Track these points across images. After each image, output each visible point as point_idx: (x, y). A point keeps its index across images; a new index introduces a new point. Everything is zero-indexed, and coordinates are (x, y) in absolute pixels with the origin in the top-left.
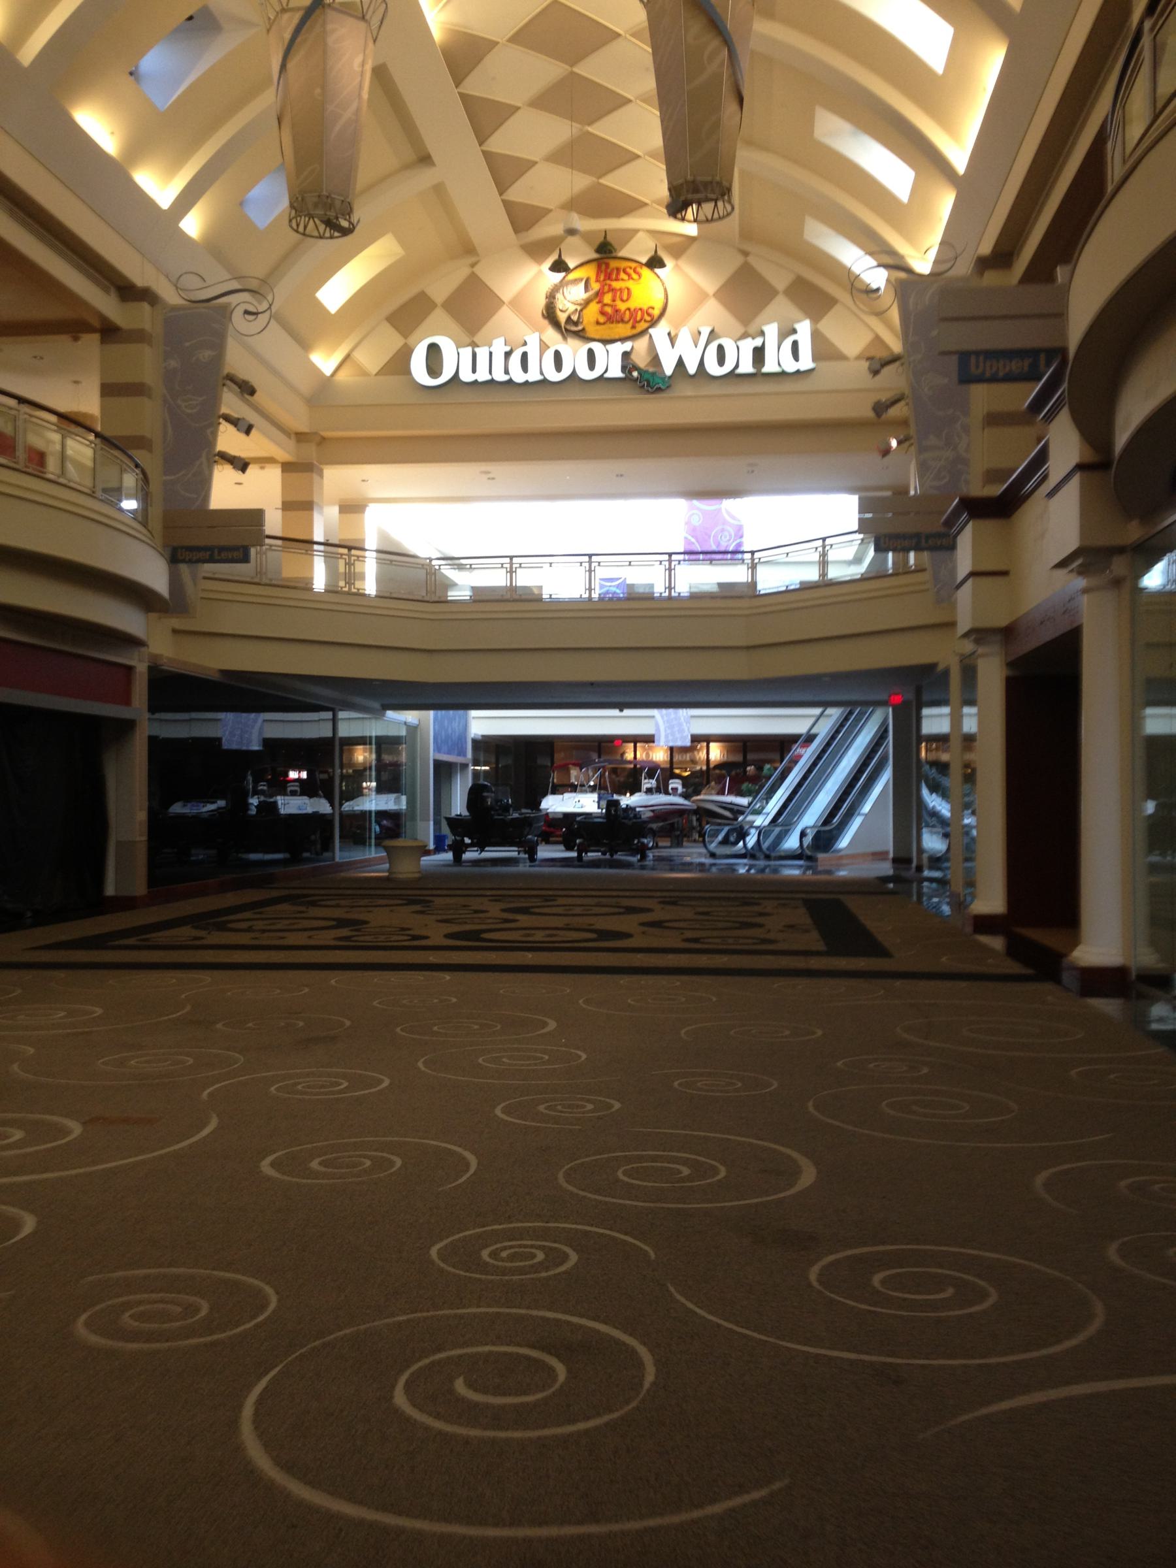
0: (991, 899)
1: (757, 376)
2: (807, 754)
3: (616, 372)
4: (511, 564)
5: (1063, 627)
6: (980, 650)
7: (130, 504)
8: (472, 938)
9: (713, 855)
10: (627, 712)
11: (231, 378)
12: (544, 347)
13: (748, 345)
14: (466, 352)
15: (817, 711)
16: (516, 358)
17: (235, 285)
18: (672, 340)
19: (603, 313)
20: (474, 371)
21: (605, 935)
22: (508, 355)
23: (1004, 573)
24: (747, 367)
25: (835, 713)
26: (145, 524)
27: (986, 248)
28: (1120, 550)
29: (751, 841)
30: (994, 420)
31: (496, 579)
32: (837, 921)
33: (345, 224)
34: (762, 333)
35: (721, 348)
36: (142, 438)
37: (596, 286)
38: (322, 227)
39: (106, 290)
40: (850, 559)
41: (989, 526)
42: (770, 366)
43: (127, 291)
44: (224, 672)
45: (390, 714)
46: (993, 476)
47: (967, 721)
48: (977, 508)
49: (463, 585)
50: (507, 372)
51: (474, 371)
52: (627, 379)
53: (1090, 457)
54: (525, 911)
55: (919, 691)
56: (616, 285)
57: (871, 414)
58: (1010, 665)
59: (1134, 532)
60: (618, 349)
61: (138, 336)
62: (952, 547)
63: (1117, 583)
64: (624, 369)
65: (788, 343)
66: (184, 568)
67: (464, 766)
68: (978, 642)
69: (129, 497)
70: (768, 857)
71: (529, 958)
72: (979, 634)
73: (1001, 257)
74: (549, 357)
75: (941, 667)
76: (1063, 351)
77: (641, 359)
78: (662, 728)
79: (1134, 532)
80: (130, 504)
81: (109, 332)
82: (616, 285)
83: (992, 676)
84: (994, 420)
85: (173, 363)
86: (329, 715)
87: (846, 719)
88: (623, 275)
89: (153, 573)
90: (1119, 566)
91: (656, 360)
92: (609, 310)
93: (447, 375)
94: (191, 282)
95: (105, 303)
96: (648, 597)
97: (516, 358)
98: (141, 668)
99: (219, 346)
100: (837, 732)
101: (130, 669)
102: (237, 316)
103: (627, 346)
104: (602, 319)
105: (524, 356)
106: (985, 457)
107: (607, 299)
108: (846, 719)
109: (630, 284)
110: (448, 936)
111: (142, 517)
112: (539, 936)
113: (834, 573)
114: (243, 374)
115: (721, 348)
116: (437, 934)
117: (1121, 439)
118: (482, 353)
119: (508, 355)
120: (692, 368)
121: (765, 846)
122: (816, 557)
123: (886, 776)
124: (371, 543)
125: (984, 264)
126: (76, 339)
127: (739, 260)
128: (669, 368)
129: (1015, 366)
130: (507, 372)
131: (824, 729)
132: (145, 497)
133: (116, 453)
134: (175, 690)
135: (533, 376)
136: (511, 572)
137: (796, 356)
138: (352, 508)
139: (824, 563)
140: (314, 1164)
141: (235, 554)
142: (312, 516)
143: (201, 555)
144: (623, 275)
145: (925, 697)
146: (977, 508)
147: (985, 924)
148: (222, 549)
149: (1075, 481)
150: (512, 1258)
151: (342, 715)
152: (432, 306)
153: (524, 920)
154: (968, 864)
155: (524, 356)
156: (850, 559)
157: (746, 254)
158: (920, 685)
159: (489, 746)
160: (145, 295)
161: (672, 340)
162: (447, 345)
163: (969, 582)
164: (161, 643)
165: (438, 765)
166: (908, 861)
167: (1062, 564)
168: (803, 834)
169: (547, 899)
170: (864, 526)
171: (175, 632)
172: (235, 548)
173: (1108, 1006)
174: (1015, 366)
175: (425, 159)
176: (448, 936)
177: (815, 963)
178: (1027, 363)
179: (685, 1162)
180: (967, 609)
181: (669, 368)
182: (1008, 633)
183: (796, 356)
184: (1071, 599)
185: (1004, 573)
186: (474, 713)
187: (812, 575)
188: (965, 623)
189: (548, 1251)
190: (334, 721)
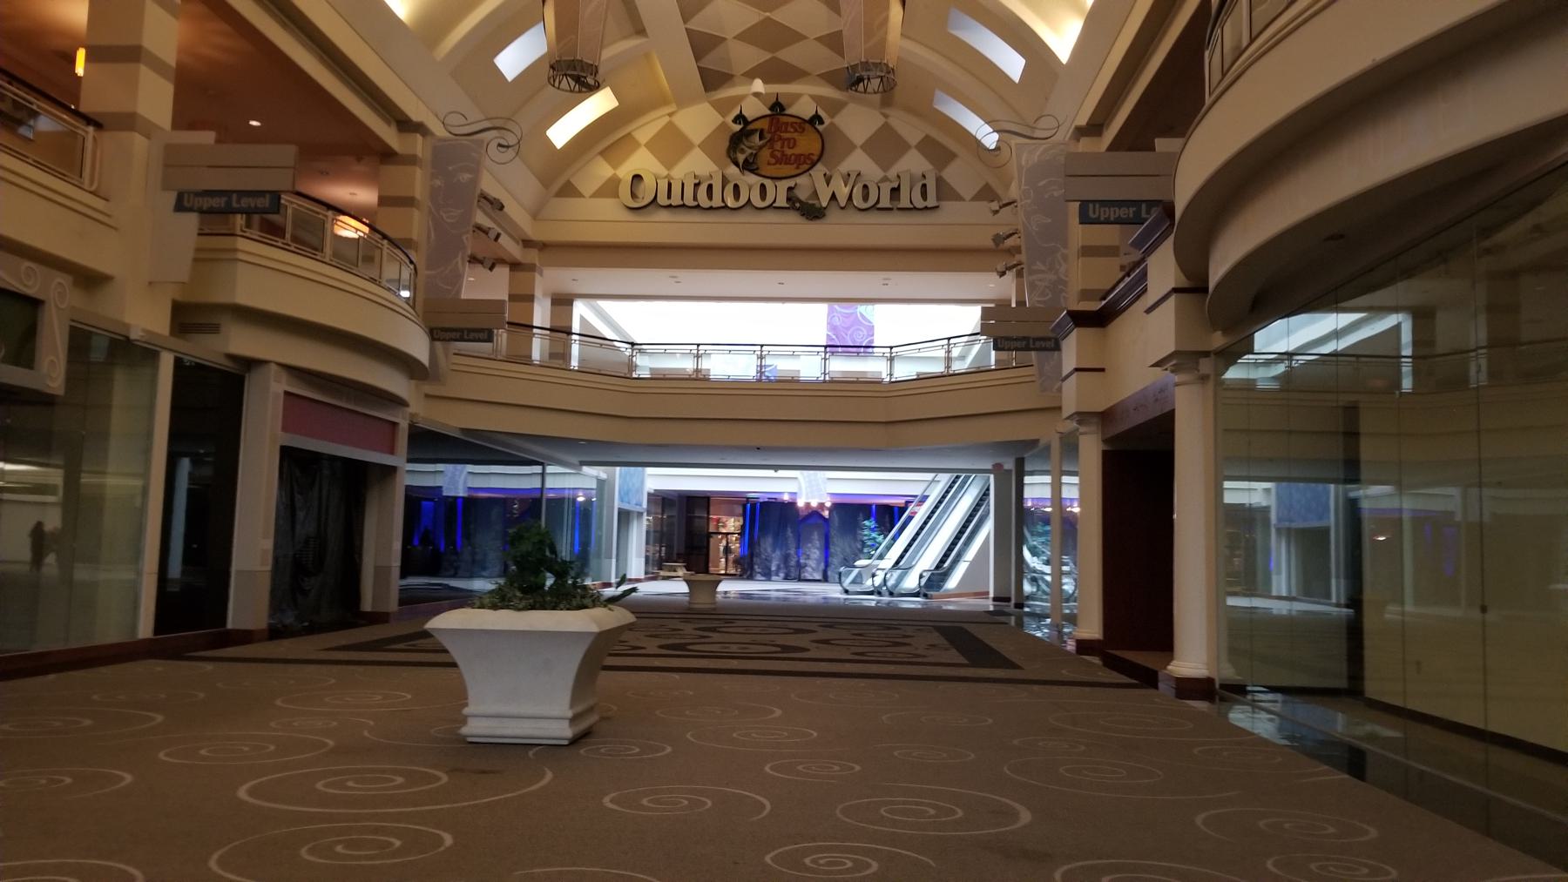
0: (1092, 629)
2: (922, 512)
4: (761, 351)
5: (1155, 411)
6: (1082, 429)
7: (405, 294)
8: (680, 649)
9: (847, 592)
10: (782, 473)
11: (484, 197)
12: (725, 181)
15: (929, 476)
17: (487, 124)
18: (828, 180)
20: (669, 197)
21: (786, 649)
22: (697, 185)
23: (1103, 370)
25: (945, 479)
26: (413, 308)
27: (1082, 120)
28: (1206, 354)
29: (878, 581)
30: (1088, 251)
31: (688, 365)
32: (961, 647)
33: (590, 81)
37: (768, 136)
38: (572, 83)
39: (389, 123)
40: (973, 354)
41: (1089, 333)
43: (405, 125)
44: (465, 431)
45: (586, 469)
46: (1086, 295)
47: (1066, 490)
48: (1081, 319)
49: (645, 365)
50: (695, 198)
51: (669, 197)
53: (1184, 282)
54: (714, 630)
55: (1020, 463)
57: (990, 244)
58: (1105, 441)
59: (1218, 340)
60: (783, 186)
61: (412, 160)
62: (1057, 348)
63: (1204, 379)
64: (788, 200)
66: (438, 344)
67: (640, 514)
68: (1080, 422)
69: (405, 288)
70: (891, 594)
71: (734, 664)
72: (1082, 417)
73: (1094, 128)
74: (730, 188)
75: (1042, 442)
76: (1169, 209)
77: (803, 194)
78: (803, 486)
79: (1218, 340)
80: (405, 294)
81: (387, 155)
83: (1091, 448)
84: (1088, 251)
85: (438, 183)
86: (538, 469)
87: (954, 482)
89: (417, 345)
90: (1206, 366)
91: (815, 194)
92: (779, 154)
94: (454, 120)
95: (387, 134)
96: (879, 382)
98: (404, 425)
99: (476, 171)
100: (947, 492)
101: (395, 424)
102: (493, 145)
103: (791, 183)
105: (710, 186)
106: (1082, 279)
107: (778, 146)
108: (954, 482)
110: (661, 647)
111: (411, 302)
112: (734, 648)
113: (958, 367)
114: (494, 191)
116: (652, 646)
117: (1217, 272)
119: (697, 185)
121: (891, 583)
122: (942, 353)
123: (988, 528)
124: (576, 327)
125: (1081, 132)
127: (882, 120)
129: (1123, 212)
130: (695, 198)
131: (935, 494)
132: (414, 288)
133: (397, 251)
134: (432, 444)
136: (761, 357)
138: (563, 302)
139: (949, 360)
140: (645, 802)
141: (481, 335)
143: (453, 335)
145: (1028, 468)
146: (1081, 319)
147: (1084, 646)
148: (470, 330)
149: (1172, 300)
150: (829, 864)
151: (550, 469)
152: (638, 145)
153: (716, 637)
155: (710, 186)
156: (973, 354)
157: (886, 116)
158: (1016, 460)
159: (663, 500)
160: (420, 128)
161: (828, 180)
163: (1074, 376)
164: (419, 407)
165: (621, 512)
166: (1008, 600)
167: (1157, 365)
168: (921, 577)
169: (727, 621)
170: (985, 329)
171: (427, 396)
172: (482, 330)
173: (1201, 705)
174: (1123, 212)
175: (641, 32)
176: (661, 647)
177: (963, 672)
178: (1132, 210)
179: (929, 805)
180: (1072, 396)
182: (1105, 417)
184: (1162, 391)
185: (1103, 370)
186: (650, 470)
187: (939, 368)
188: (1069, 407)
189: (854, 861)
190: (543, 475)
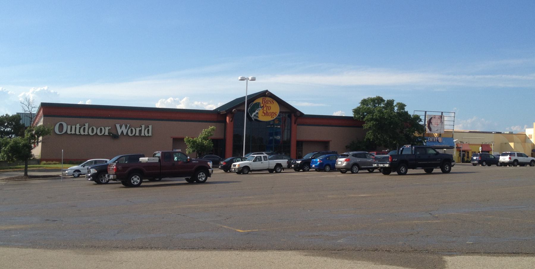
1: (75, 134)
3: (107, 134)
13: (138, 129)
14: (69, 127)
22: (80, 128)
24: (137, 134)
34: (141, 127)
42: (143, 134)
50: (80, 132)
56: (267, 105)
64: (109, 133)
82: (267, 105)
92: (265, 112)
104: (263, 114)
107: (265, 109)
109: (271, 105)
115: (132, 130)
118: (74, 127)
120: (125, 134)
126: (7, 115)
128: (119, 134)
130: (80, 132)
135: (86, 133)
137: (148, 133)
154: (516, 155)
162: (65, 125)
181: (119, 134)
183: (148, 133)
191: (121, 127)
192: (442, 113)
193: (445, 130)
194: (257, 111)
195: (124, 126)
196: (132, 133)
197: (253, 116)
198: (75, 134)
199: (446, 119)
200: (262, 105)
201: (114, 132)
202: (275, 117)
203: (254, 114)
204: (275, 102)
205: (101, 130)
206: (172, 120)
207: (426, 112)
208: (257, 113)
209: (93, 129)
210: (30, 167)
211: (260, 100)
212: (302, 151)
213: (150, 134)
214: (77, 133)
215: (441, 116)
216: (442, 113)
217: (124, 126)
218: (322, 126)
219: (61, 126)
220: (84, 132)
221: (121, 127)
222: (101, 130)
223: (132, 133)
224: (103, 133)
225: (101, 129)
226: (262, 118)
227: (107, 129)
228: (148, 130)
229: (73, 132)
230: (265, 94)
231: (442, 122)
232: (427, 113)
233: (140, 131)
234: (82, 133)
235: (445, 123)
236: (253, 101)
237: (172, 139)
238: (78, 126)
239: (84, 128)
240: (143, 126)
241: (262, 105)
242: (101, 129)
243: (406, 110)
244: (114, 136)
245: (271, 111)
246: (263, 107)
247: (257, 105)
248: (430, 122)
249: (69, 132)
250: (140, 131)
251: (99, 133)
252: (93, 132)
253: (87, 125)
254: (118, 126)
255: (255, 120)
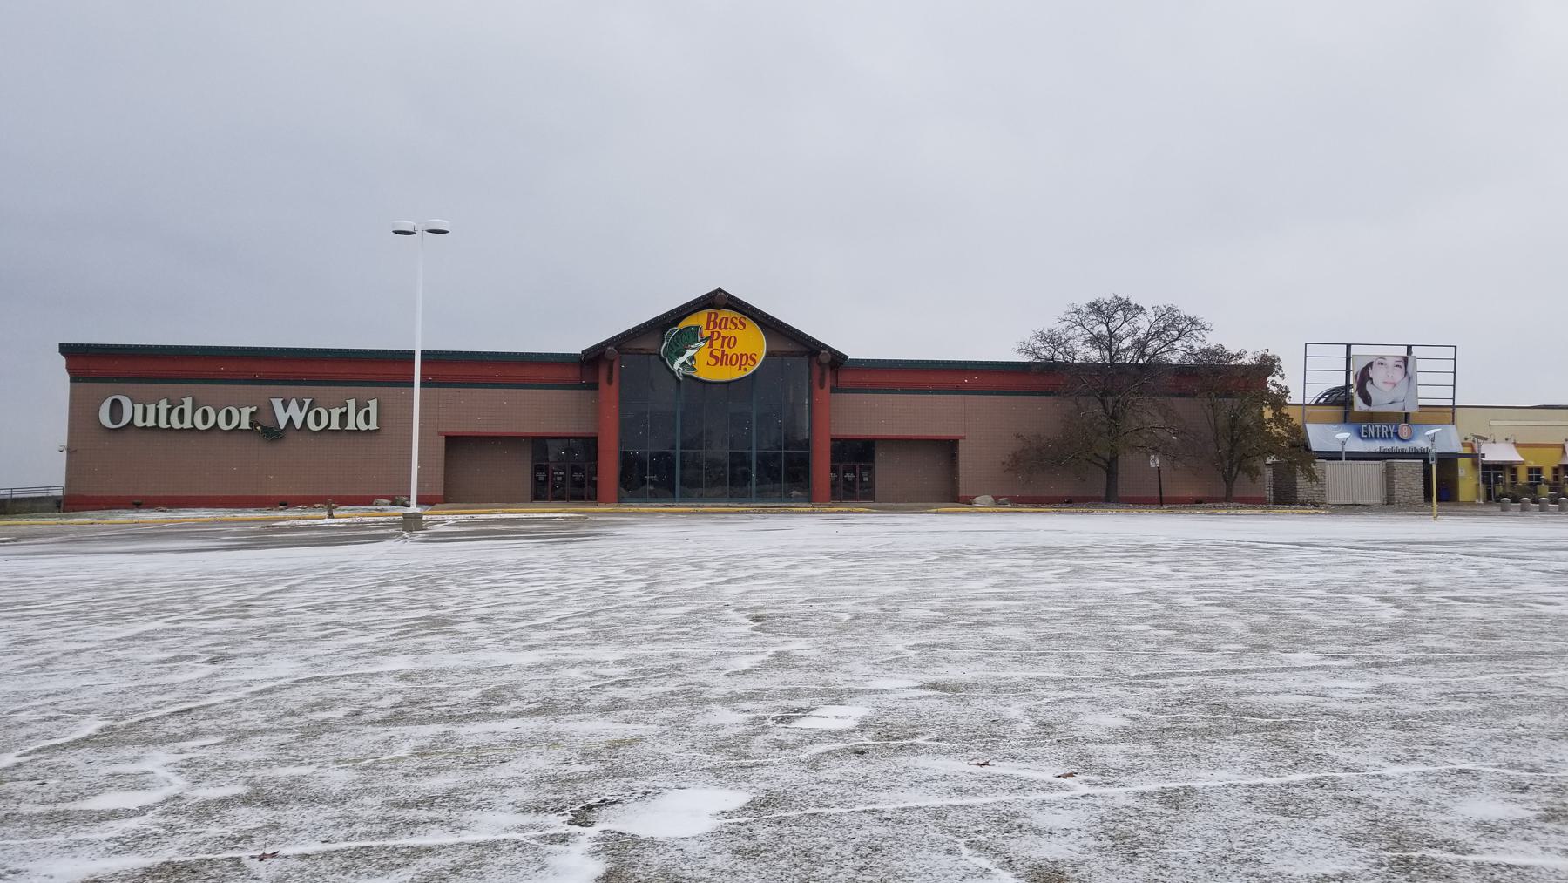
1: (343, 430)
3: (245, 425)
13: (336, 413)
14: (139, 408)
16: (175, 412)
19: (712, 355)
22: (169, 411)
24: (335, 425)
35: (318, 413)
36: (1236, 385)
42: (351, 426)
50: (168, 422)
52: (252, 430)
56: (724, 333)
65: (362, 413)
82: (724, 333)
88: (730, 325)
92: (719, 354)
93: (126, 420)
97: (175, 412)
104: (713, 361)
107: (717, 344)
109: (736, 333)
115: (318, 413)
118: (151, 409)
130: (168, 422)
135: (187, 425)
137: (367, 421)
142: (68, 480)
144: (730, 325)
183: (367, 421)
191: (286, 406)
192: (1409, 347)
193: (1421, 403)
194: (689, 353)
195: (294, 405)
196: (318, 422)
197: (677, 365)
198: (157, 427)
199: (1421, 365)
200: (706, 334)
201: (267, 423)
202: (751, 370)
203: (681, 360)
204: (748, 322)
205: (229, 415)
206: (926, 392)
207: (1349, 346)
208: (692, 358)
209: (205, 413)
210: (823, 374)
211: (699, 320)
212: (871, 470)
213: (373, 426)
214: (163, 424)
215: (1405, 360)
216: (1409, 347)
217: (294, 405)
218: (540, 386)
219: (116, 406)
220: (181, 421)
221: (286, 406)
222: (229, 415)
223: (318, 422)
224: (234, 424)
225: (229, 413)
226: (708, 371)
227: (246, 411)
228: (367, 413)
229: (151, 422)
230: (717, 301)
231: (1409, 377)
232: (1354, 351)
233: (343, 416)
234: (176, 424)
235: (1421, 378)
236: (677, 322)
237: (442, 440)
238: (163, 406)
239: (182, 412)
240: (352, 404)
241: (706, 334)
242: (229, 413)
243: (1212, 340)
244: (266, 431)
245: (738, 350)
246: (711, 338)
247: (693, 335)
248: (1364, 377)
249: (139, 422)
250: (343, 416)
251: (223, 425)
252: (205, 421)
253: (373, 405)
254: (277, 404)
255: (685, 376)
